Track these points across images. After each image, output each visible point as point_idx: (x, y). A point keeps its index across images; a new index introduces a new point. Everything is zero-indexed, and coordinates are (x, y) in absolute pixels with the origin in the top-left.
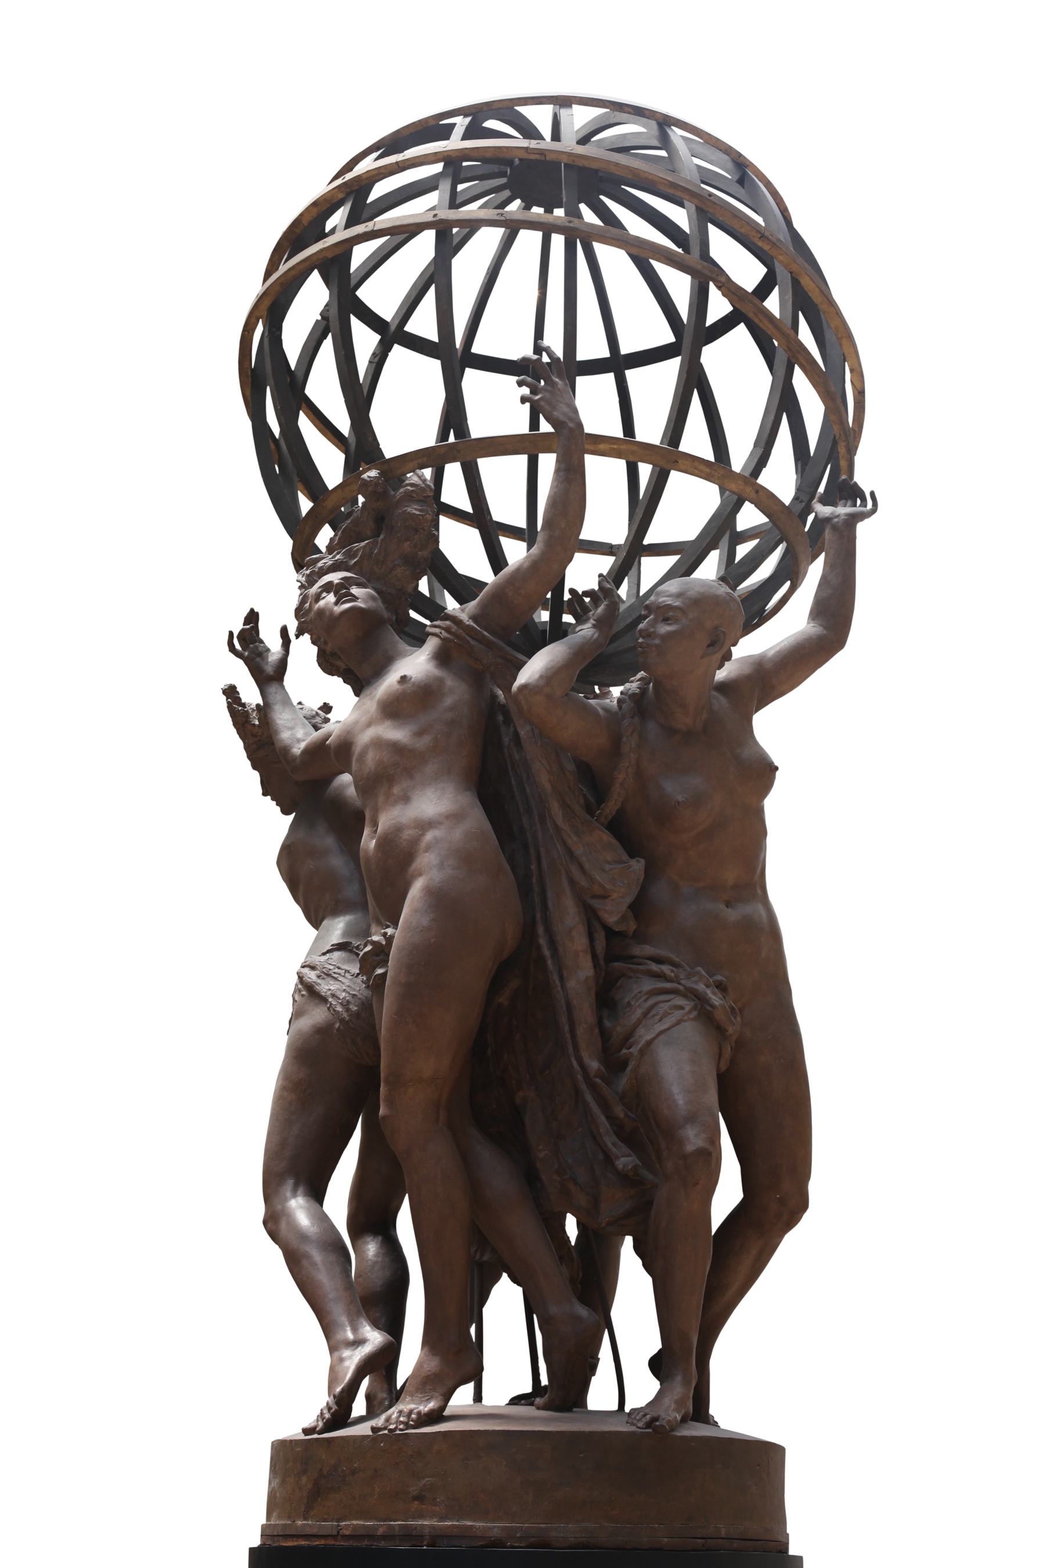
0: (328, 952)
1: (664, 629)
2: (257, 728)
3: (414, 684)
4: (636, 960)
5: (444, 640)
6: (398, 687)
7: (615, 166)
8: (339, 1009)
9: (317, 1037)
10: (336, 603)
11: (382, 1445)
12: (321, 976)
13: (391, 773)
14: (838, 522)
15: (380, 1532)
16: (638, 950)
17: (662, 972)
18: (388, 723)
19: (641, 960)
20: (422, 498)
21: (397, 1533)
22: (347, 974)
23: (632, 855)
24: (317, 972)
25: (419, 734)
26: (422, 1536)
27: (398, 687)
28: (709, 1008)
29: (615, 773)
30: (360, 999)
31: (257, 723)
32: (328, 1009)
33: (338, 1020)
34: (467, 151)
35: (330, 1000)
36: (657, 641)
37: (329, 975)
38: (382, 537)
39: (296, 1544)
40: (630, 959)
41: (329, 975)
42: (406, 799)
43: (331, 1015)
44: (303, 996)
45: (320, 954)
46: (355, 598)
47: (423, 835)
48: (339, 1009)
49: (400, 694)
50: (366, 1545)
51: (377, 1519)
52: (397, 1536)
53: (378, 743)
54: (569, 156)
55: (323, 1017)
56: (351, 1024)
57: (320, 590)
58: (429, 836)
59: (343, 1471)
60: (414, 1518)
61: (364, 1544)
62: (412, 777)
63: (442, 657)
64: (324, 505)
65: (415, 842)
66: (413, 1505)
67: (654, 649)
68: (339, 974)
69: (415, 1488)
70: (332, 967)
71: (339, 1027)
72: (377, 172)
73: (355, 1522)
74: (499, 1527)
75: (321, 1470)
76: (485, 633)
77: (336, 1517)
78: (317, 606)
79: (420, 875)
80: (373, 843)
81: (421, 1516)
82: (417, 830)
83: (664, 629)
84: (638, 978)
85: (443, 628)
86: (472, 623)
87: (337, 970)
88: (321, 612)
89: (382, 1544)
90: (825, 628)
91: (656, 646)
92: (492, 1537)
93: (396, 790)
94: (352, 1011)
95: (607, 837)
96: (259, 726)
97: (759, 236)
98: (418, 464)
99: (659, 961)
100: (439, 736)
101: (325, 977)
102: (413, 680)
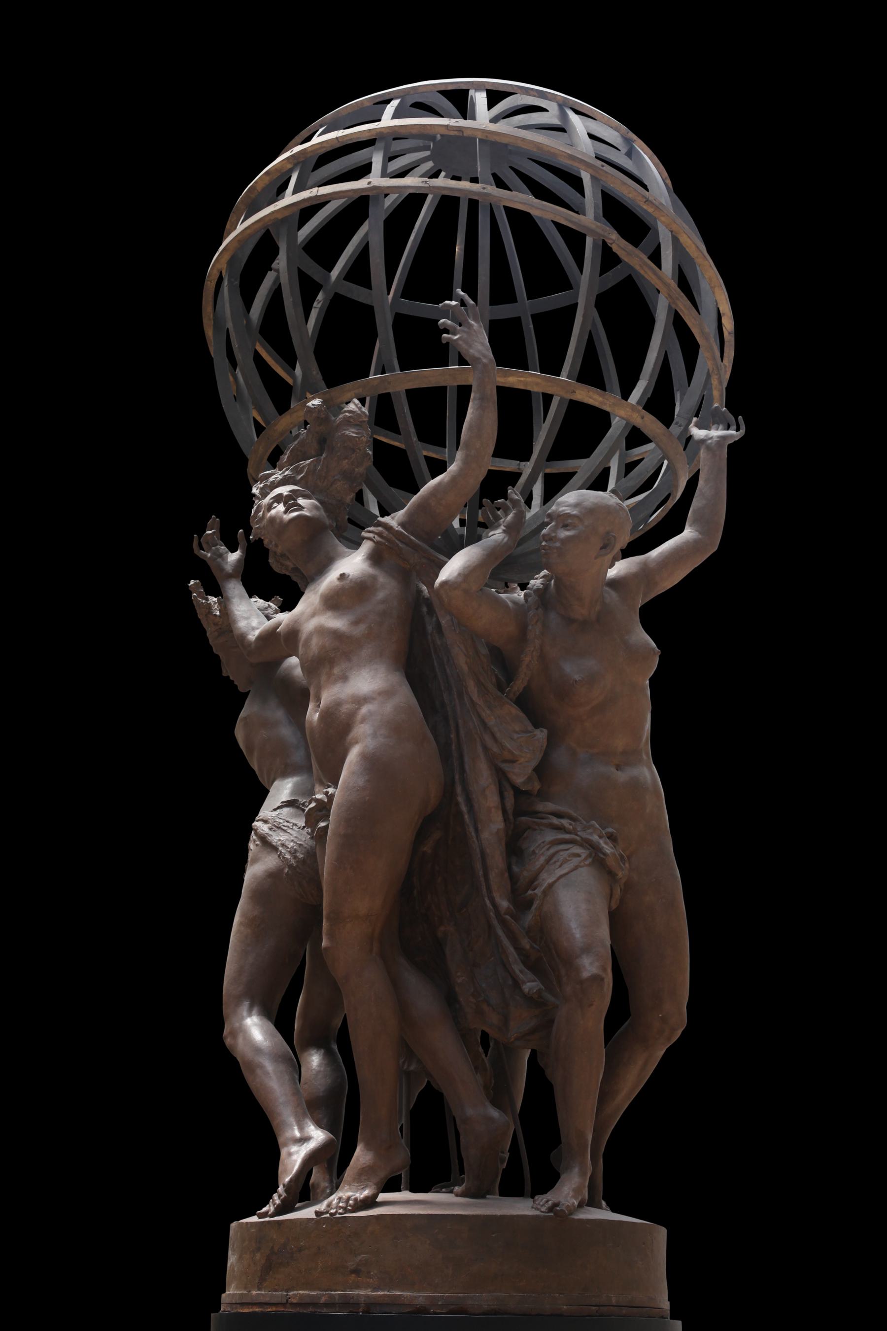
0: (279, 808)
1: (564, 534)
2: (218, 618)
3: (351, 581)
4: (540, 815)
5: (377, 543)
6: (337, 583)
7: (522, 141)
8: (288, 856)
9: (269, 880)
10: (286, 512)
11: (324, 1226)
12: (272, 828)
13: (332, 656)
14: (711, 443)
15: (323, 1300)
16: (542, 807)
17: (562, 825)
18: (329, 614)
19: (544, 815)
20: (358, 423)
21: (337, 1301)
22: (294, 827)
23: (536, 726)
24: (269, 825)
25: (356, 623)
26: (358, 1304)
27: (337, 583)
28: (602, 856)
29: (522, 656)
30: (305, 848)
31: (218, 613)
32: (279, 856)
33: (287, 866)
34: (396, 128)
35: (280, 849)
36: (558, 544)
37: (279, 828)
38: (324, 455)
39: (251, 1310)
40: (535, 814)
41: (279, 828)
42: (344, 678)
43: (281, 861)
44: (257, 845)
45: (272, 810)
46: (301, 508)
47: (359, 709)
48: (288, 856)
49: (340, 589)
50: (310, 1312)
51: (320, 1289)
52: (337, 1304)
53: (321, 631)
54: (483, 132)
55: (274, 863)
56: (298, 870)
57: (271, 501)
58: (364, 710)
59: (291, 1249)
60: (352, 1289)
61: (309, 1310)
62: (349, 660)
63: (375, 558)
64: (275, 428)
65: (352, 715)
66: (350, 1278)
67: (555, 551)
68: (288, 827)
69: (352, 1263)
70: (281, 821)
71: (288, 872)
72: (320, 146)
73: (301, 1292)
74: (423, 1296)
75: (272, 1248)
76: (412, 537)
77: (285, 1288)
78: (269, 515)
79: (357, 743)
80: (317, 716)
81: (358, 1287)
82: (354, 705)
83: (564, 534)
84: (542, 830)
85: (376, 533)
86: (400, 529)
87: (286, 824)
88: (273, 520)
89: (325, 1310)
90: (700, 533)
91: (557, 548)
92: (418, 1305)
93: (336, 671)
94: (299, 859)
95: (515, 710)
96: (220, 616)
97: (645, 200)
98: (355, 394)
99: (559, 815)
100: (372, 625)
101: (276, 829)
102: (350, 577)
